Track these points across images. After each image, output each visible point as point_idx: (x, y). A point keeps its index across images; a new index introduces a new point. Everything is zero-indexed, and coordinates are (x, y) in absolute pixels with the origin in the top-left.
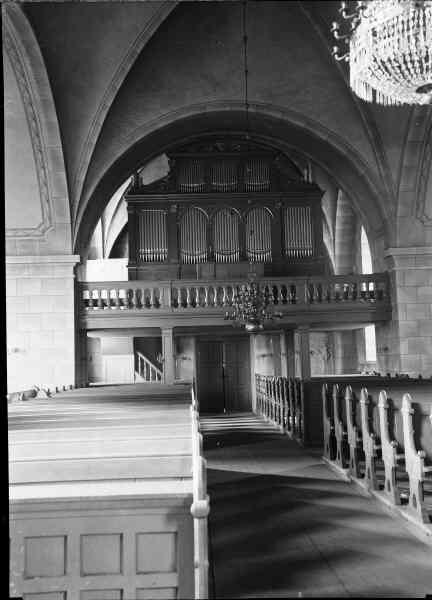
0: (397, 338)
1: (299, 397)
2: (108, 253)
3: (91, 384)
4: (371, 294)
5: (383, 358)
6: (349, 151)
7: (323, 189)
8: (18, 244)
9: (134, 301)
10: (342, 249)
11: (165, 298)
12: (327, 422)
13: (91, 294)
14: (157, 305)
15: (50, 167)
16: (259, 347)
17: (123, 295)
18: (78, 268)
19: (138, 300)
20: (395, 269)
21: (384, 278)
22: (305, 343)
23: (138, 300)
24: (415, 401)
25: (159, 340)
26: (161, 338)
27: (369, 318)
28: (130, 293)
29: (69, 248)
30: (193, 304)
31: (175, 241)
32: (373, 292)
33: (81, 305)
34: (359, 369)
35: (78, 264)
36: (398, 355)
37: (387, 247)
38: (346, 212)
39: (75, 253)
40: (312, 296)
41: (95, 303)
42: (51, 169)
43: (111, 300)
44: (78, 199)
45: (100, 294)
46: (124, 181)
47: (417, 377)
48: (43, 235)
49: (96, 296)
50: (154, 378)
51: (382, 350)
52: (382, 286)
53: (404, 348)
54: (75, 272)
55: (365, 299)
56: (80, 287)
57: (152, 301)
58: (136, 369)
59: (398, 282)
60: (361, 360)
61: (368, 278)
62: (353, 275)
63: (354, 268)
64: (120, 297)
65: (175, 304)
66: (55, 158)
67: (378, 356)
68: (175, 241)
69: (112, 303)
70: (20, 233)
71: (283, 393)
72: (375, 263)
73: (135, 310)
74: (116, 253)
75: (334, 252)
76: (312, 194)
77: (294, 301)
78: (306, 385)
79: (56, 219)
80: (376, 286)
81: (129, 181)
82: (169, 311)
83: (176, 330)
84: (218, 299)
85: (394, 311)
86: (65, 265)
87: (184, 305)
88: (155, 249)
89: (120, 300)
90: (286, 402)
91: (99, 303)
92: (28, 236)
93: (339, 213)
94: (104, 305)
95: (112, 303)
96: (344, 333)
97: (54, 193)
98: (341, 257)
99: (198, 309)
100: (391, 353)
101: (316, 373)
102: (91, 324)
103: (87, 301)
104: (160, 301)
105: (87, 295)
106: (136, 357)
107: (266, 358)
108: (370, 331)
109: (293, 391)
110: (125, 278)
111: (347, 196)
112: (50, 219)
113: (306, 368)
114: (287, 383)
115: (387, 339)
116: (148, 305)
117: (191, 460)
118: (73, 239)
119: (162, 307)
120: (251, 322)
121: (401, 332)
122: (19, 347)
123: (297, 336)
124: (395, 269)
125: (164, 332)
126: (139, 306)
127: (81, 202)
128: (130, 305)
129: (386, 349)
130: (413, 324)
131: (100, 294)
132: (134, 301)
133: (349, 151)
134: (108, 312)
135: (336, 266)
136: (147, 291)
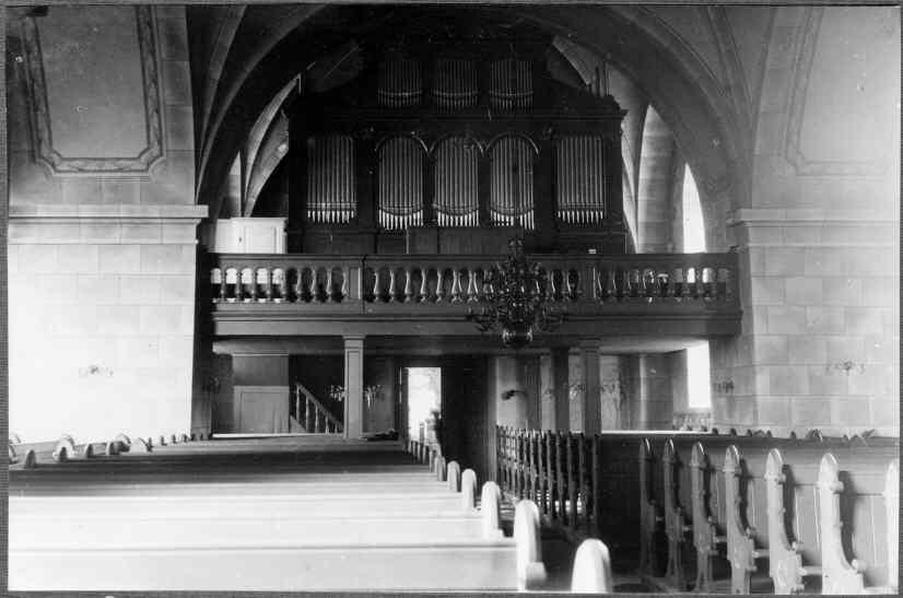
0: (751, 365)
1: (588, 465)
2: (252, 201)
3: (215, 436)
4: (707, 288)
5: (723, 401)
6: (714, 34)
7: (622, 107)
8: (103, 184)
9: (298, 290)
10: (648, 212)
11: (353, 286)
12: (647, 510)
13: (225, 275)
14: (338, 297)
15: (163, 51)
16: (504, 380)
17: (279, 276)
18: (205, 229)
19: (321, 287)
20: (750, 245)
21: (729, 262)
22: (592, 371)
23: (305, 287)
24: (844, 468)
25: (339, 362)
26: (343, 356)
27: (703, 332)
28: (290, 276)
29: (190, 193)
30: (400, 297)
31: (368, 198)
32: (708, 284)
33: (207, 295)
34: (675, 422)
35: (204, 220)
36: (751, 399)
37: (736, 207)
38: (659, 150)
39: (200, 201)
40: (604, 291)
41: (230, 290)
42: (164, 55)
43: (259, 287)
44: (208, 110)
45: (240, 275)
46: (285, 84)
47: (787, 436)
48: (147, 170)
49: (232, 278)
50: (322, 430)
51: (723, 387)
52: (724, 273)
53: (762, 382)
54: (198, 236)
55: (696, 297)
56: (207, 260)
57: (329, 292)
58: (292, 412)
59: (753, 270)
60: (677, 409)
61: (701, 261)
62: (667, 258)
63: (670, 246)
64: (276, 281)
65: (368, 297)
66: (173, 39)
67: (714, 398)
68: (368, 198)
69: (260, 293)
70: (108, 166)
71: (553, 459)
72: (712, 235)
73: (300, 306)
74: (263, 209)
75: (636, 216)
76: (601, 121)
77: (574, 297)
78: (588, 442)
79: (170, 143)
80: (715, 275)
81: (292, 84)
82: (357, 308)
83: (371, 342)
84: (444, 289)
85: (744, 317)
86: (180, 221)
87: (385, 297)
88: (332, 207)
89: (274, 287)
90: (560, 474)
91: (238, 292)
92: (120, 170)
93: (645, 152)
94: (245, 294)
95: (260, 293)
96: (652, 358)
97: (166, 95)
98: (648, 226)
99: (408, 306)
100: (740, 392)
101: (609, 428)
102: (222, 328)
103: (218, 286)
104: (344, 291)
105: (217, 278)
106: (293, 389)
107: (513, 400)
108: (698, 356)
109: (544, 451)
110: (280, 249)
111: (666, 118)
112: (160, 143)
113: (592, 414)
114: (565, 442)
115: (730, 369)
116: (322, 297)
117: (513, 555)
118: (197, 183)
119: (346, 299)
120: (508, 326)
121: (758, 356)
122: (95, 364)
123: (574, 361)
124: (750, 245)
125: (348, 344)
126: (307, 297)
127: (214, 116)
128: (291, 297)
129: (730, 386)
130: (777, 341)
131: (240, 275)
132: (298, 290)
133: (714, 34)
134: (252, 308)
135: (639, 242)
136: (306, 273)
